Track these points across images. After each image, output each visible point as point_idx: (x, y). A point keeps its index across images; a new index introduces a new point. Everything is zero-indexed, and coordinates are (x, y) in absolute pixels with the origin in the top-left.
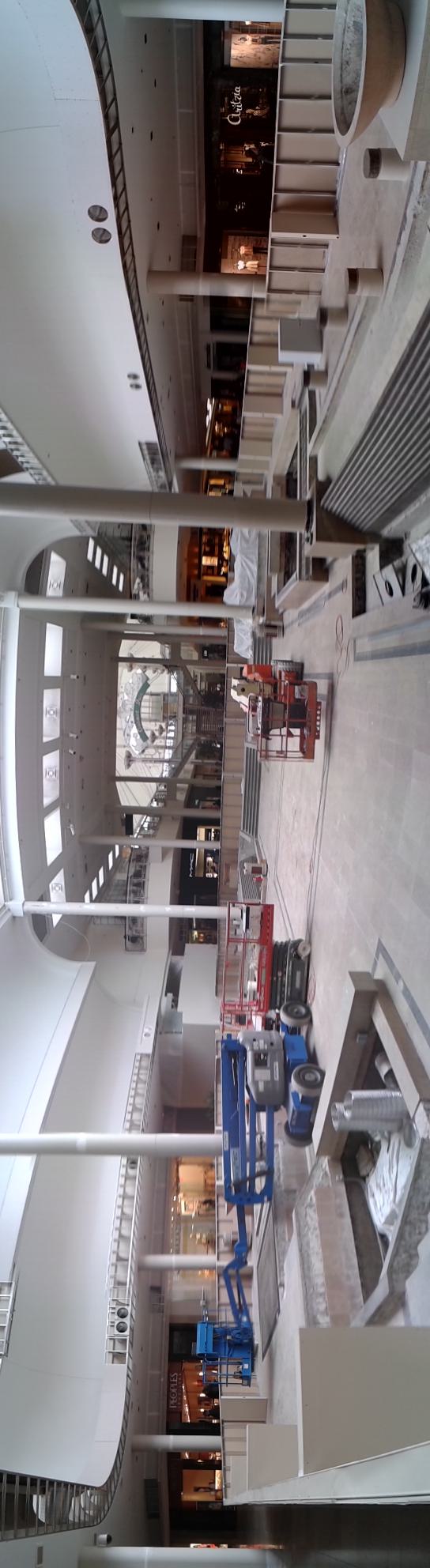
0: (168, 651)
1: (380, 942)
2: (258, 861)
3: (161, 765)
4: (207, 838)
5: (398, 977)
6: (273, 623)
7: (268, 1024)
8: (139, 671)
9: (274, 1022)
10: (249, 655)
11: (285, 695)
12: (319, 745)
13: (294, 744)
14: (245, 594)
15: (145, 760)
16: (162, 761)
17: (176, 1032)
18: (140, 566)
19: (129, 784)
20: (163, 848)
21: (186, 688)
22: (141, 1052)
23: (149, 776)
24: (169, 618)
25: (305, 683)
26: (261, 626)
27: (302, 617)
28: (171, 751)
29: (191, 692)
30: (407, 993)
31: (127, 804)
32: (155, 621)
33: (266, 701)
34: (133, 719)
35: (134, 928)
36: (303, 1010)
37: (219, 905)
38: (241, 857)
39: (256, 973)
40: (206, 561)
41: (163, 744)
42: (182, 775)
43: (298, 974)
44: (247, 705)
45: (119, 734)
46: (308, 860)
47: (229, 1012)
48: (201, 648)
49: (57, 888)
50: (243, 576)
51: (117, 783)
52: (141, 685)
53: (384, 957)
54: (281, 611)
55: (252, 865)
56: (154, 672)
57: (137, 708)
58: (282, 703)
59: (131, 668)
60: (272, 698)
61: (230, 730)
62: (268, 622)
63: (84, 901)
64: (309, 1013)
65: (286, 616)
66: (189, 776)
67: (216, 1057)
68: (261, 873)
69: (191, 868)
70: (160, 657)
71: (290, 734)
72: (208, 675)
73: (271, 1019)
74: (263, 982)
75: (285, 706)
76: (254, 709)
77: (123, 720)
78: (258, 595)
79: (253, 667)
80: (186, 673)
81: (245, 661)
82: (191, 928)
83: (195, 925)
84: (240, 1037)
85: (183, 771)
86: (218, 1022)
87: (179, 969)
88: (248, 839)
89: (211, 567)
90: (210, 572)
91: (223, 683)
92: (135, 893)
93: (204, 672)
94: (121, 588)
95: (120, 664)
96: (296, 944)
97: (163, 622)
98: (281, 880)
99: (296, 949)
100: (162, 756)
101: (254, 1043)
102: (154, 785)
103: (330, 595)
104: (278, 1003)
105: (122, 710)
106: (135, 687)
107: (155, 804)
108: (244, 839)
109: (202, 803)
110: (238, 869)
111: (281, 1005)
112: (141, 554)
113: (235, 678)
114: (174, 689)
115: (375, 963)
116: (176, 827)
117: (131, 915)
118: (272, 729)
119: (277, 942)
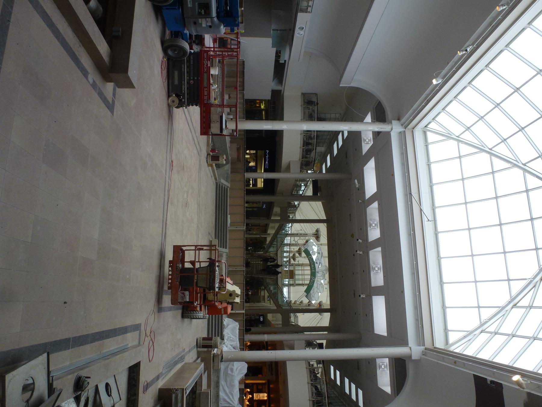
0: (292, 319)
1: (112, 112)
2: (214, 165)
3: (293, 232)
4: (255, 181)
5: (94, 85)
6: (205, 349)
7: (200, 40)
8: (313, 302)
9: (194, 42)
10: (227, 321)
11: (197, 293)
12: (169, 256)
13: (189, 256)
14: (229, 372)
15: (305, 235)
16: (292, 235)
17: (277, 30)
18: (319, 387)
19: (316, 218)
20: (289, 172)
21: (276, 291)
22: (307, 14)
23: (302, 224)
24: (292, 348)
25: (181, 303)
26: (216, 347)
27: (181, 357)
28: (285, 242)
29: (272, 288)
30: (85, 74)
31: (317, 202)
32: (303, 343)
33: (212, 287)
34: (316, 265)
35: (310, 111)
36: (170, 52)
37: (244, 130)
38: (228, 167)
39: (212, 81)
40: (264, 396)
41: (292, 247)
42: (277, 225)
43: (176, 82)
44: (227, 283)
45: (326, 253)
46: (175, 170)
47: (232, 50)
48: (266, 323)
49: (367, 140)
50: (231, 386)
51: (325, 218)
52: (312, 292)
53: (108, 101)
54: (199, 360)
55: (220, 162)
56: (301, 302)
57: (313, 274)
58: (200, 287)
59: (320, 304)
60: (207, 291)
61: (240, 262)
62: (210, 349)
63: (348, 132)
64: (165, 50)
65: (195, 357)
66: (271, 225)
67: (243, 9)
68: (212, 156)
69: (267, 157)
70: (298, 314)
71: (193, 263)
72: (259, 301)
73: (197, 44)
74: (205, 75)
75: (197, 285)
76: (222, 281)
77: (323, 264)
78: (218, 371)
79: (223, 313)
80: (276, 302)
81: (231, 316)
82: (266, 110)
83: (264, 113)
84: (223, 29)
85: (276, 228)
86: (242, 40)
87: (275, 80)
88: (223, 181)
89: (260, 391)
90: (260, 387)
91: (247, 295)
92: (310, 138)
93: (262, 304)
94: (332, 368)
95: (329, 307)
96: (180, 105)
97: (296, 344)
98: (196, 152)
99: (180, 101)
100: (293, 238)
101: (210, 24)
102: (298, 217)
103: (158, 378)
104: (192, 58)
105: (325, 272)
106: (316, 290)
107: (296, 203)
108: (227, 181)
109: (261, 206)
110: (230, 158)
111: (189, 56)
112: (319, 398)
113: (238, 303)
114: (285, 290)
115: (114, 94)
116: (280, 187)
117: (314, 122)
118: (207, 267)
119: (197, 106)
